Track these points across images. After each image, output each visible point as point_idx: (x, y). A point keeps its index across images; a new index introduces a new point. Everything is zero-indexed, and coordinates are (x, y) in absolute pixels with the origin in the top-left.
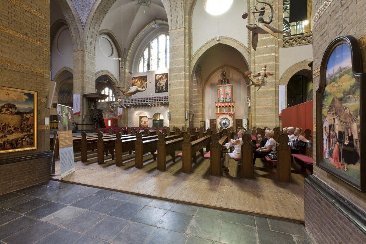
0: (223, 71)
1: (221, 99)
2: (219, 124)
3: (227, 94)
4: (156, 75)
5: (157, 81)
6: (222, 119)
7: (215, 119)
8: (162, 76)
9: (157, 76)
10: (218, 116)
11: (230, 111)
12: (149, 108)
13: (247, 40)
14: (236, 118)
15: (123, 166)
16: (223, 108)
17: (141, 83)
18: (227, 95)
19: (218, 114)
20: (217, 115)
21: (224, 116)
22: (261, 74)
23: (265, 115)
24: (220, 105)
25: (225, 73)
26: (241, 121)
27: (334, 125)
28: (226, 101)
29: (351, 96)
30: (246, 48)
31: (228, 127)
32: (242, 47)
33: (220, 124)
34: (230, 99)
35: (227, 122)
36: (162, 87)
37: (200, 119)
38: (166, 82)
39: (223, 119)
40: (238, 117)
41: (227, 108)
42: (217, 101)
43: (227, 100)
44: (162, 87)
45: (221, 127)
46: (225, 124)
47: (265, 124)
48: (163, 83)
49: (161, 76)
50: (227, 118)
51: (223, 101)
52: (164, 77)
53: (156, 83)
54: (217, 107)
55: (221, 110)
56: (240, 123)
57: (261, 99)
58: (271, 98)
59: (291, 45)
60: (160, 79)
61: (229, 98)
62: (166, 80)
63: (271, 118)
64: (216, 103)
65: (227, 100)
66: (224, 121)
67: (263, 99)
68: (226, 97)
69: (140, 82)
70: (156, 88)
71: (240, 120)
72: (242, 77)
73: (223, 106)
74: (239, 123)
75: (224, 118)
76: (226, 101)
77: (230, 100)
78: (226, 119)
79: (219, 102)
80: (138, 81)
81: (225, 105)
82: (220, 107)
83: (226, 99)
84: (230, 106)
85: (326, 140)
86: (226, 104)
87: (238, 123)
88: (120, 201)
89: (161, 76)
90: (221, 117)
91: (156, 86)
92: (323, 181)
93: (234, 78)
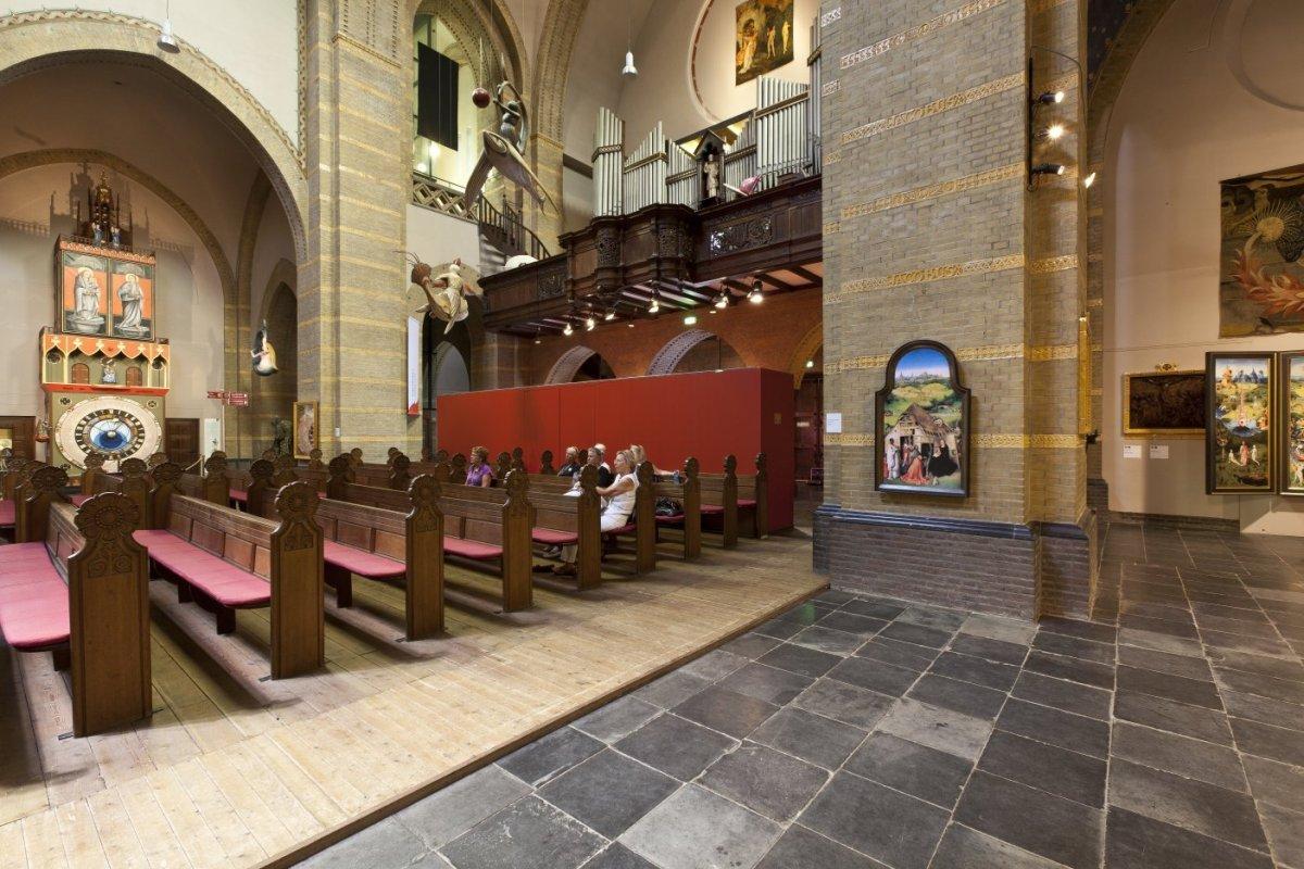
0: (83, 178)
1: (85, 314)
3: (127, 299)
6: (92, 416)
10: (65, 401)
11: (140, 379)
13: (295, 116)
14: (167, 416)
15: (52, 791)
16: (95, 366)
18: (125, 304)
19: (66, 389)
22: (452, 282)
23: (371, 410)
24: (78, 343)
25: (110, 195)
26: (193, 426)
27: (912, 437)
28: (116, 331)
29: (945, 407)
30: (292, 145)
31: (130, 453)
32: (274, 134)
33: (81, 439)
35: (124, 431)
39: (121, 416)
40: (181, 410)
41: (120, 367)
43: (123, 326)
45: (94, 459)
46: (109, 441)
47: (388, 439)
50: (123, 413)
51: (102, 328)
56: (186, 437)
57: (356, 351)
58: (387, 355)
59: (432, 205)
63: (388, 419)
65: (123, 326)
66: (107, 426)
67: (363, 353)
68: (119, 312)
71: (187, 423)
72: (198, 238)
73: (99, 355)
74: (181, 435)
75: (106, 412)
76: (116, 331)
77: (145, 329)
82: (76, 353)
83: (118, 319)
85: (894, 456)
86: (121, 347)
90: (86, 406)
93: (151, 232)
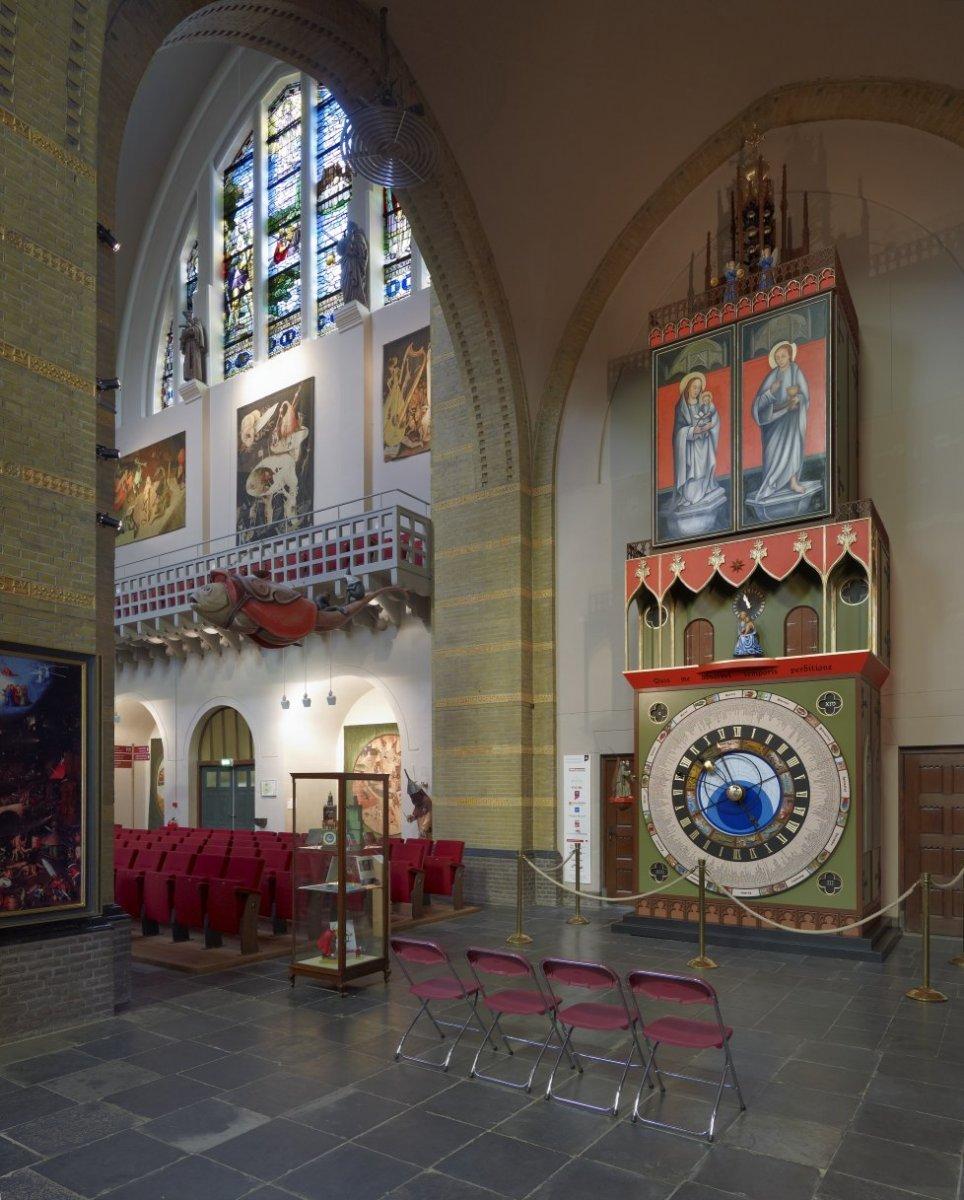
2: (669, 809)
4: (243, 412)
5: (246, 461)
7: (630, 750)
8: (275, 418)
9: (248, 420)
12: (174, 668)
17: (159, 491)
20: (651, 697)
21: (734, 708)
34: (811, 471)
36: (279, 500)
37: (496, 749)
38: (303, 453)
41: (772, 612)
42: (644, 533)
44: (279, 500)
48: (282, 465)
49: (271, 411)
52: (287, 420)
53: (242, 477)
54: (645, 599)
55: (695, 639)
60: (265, 439)
61: (796, 465)
62: (300, 436)
64: (633, 551)
65: (765, 496)
66: (744, 770)
69: (157, 484)
70: (243, 520)
78: (757, 742)
79: (667, 541)
80: (143, 483)
81: (737, 567)
83: (755, 480)
84: (806, 575)
87: (933, 800)
88: (649, 1100)
89: (271, 411)
91: (243, 498)
92: (141, 261)
